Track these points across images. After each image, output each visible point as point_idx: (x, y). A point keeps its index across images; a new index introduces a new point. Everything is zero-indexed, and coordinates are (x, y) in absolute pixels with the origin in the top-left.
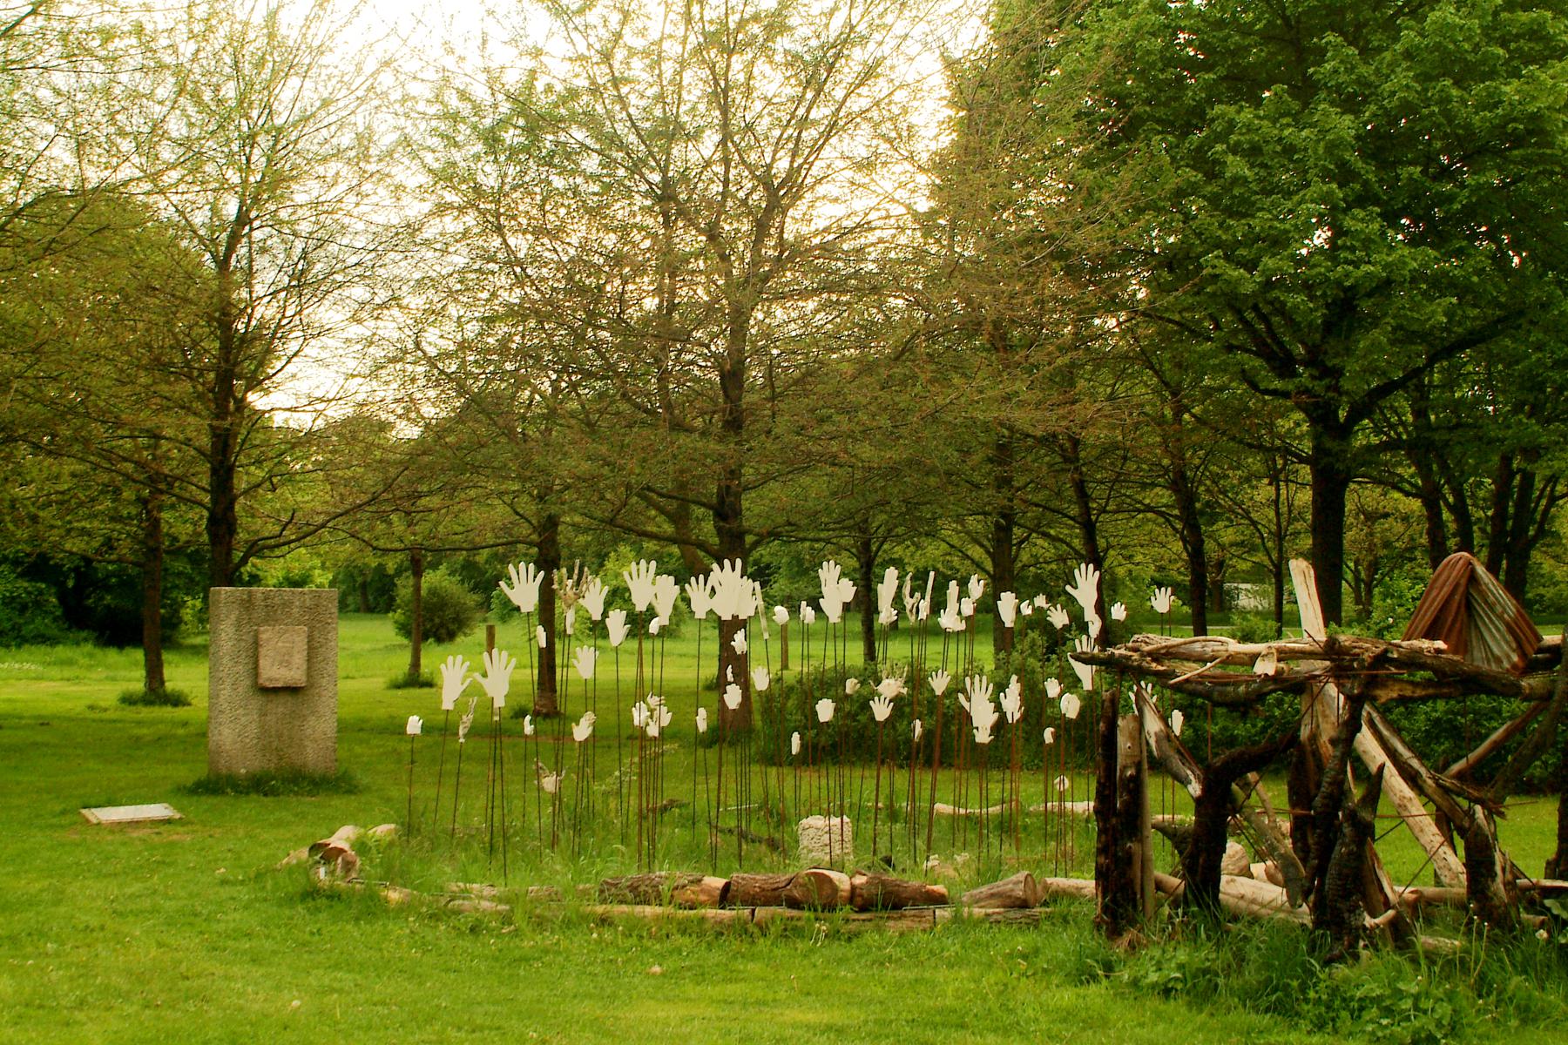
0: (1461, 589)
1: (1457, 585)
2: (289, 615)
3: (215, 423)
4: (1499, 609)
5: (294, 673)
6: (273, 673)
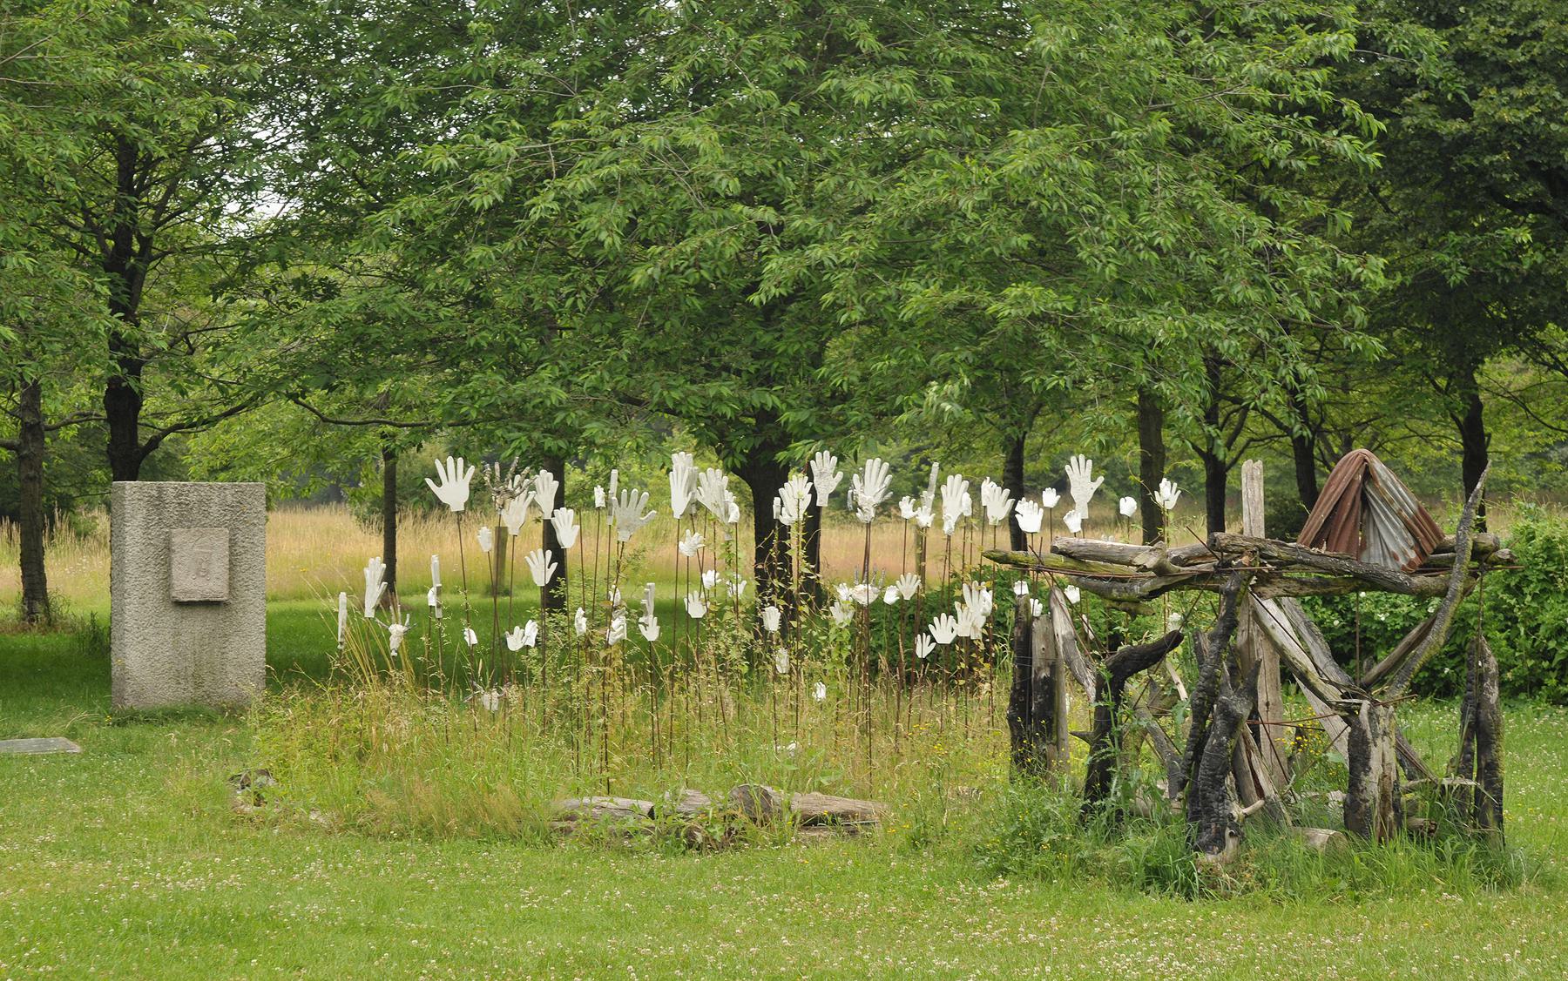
0: (1356, 486)
1: (1352, 481)
2: (206, 514)
3: (1375, 830)
4: (1396, 507)
5: (215, 587)
6: (188, 584)
